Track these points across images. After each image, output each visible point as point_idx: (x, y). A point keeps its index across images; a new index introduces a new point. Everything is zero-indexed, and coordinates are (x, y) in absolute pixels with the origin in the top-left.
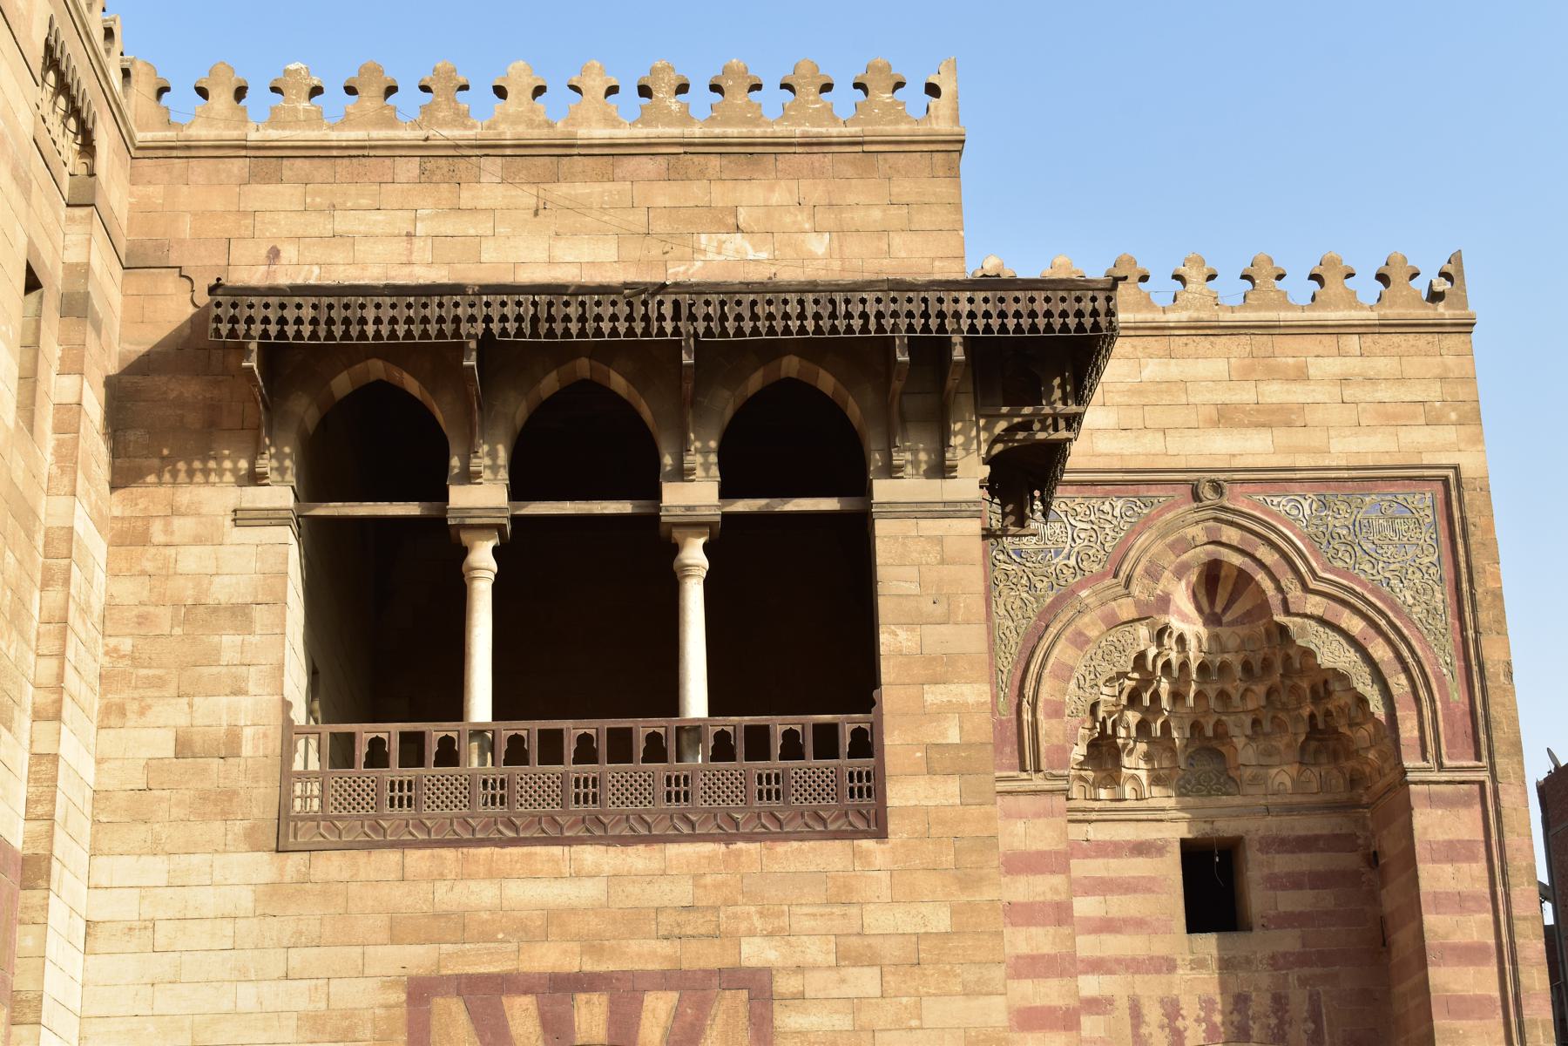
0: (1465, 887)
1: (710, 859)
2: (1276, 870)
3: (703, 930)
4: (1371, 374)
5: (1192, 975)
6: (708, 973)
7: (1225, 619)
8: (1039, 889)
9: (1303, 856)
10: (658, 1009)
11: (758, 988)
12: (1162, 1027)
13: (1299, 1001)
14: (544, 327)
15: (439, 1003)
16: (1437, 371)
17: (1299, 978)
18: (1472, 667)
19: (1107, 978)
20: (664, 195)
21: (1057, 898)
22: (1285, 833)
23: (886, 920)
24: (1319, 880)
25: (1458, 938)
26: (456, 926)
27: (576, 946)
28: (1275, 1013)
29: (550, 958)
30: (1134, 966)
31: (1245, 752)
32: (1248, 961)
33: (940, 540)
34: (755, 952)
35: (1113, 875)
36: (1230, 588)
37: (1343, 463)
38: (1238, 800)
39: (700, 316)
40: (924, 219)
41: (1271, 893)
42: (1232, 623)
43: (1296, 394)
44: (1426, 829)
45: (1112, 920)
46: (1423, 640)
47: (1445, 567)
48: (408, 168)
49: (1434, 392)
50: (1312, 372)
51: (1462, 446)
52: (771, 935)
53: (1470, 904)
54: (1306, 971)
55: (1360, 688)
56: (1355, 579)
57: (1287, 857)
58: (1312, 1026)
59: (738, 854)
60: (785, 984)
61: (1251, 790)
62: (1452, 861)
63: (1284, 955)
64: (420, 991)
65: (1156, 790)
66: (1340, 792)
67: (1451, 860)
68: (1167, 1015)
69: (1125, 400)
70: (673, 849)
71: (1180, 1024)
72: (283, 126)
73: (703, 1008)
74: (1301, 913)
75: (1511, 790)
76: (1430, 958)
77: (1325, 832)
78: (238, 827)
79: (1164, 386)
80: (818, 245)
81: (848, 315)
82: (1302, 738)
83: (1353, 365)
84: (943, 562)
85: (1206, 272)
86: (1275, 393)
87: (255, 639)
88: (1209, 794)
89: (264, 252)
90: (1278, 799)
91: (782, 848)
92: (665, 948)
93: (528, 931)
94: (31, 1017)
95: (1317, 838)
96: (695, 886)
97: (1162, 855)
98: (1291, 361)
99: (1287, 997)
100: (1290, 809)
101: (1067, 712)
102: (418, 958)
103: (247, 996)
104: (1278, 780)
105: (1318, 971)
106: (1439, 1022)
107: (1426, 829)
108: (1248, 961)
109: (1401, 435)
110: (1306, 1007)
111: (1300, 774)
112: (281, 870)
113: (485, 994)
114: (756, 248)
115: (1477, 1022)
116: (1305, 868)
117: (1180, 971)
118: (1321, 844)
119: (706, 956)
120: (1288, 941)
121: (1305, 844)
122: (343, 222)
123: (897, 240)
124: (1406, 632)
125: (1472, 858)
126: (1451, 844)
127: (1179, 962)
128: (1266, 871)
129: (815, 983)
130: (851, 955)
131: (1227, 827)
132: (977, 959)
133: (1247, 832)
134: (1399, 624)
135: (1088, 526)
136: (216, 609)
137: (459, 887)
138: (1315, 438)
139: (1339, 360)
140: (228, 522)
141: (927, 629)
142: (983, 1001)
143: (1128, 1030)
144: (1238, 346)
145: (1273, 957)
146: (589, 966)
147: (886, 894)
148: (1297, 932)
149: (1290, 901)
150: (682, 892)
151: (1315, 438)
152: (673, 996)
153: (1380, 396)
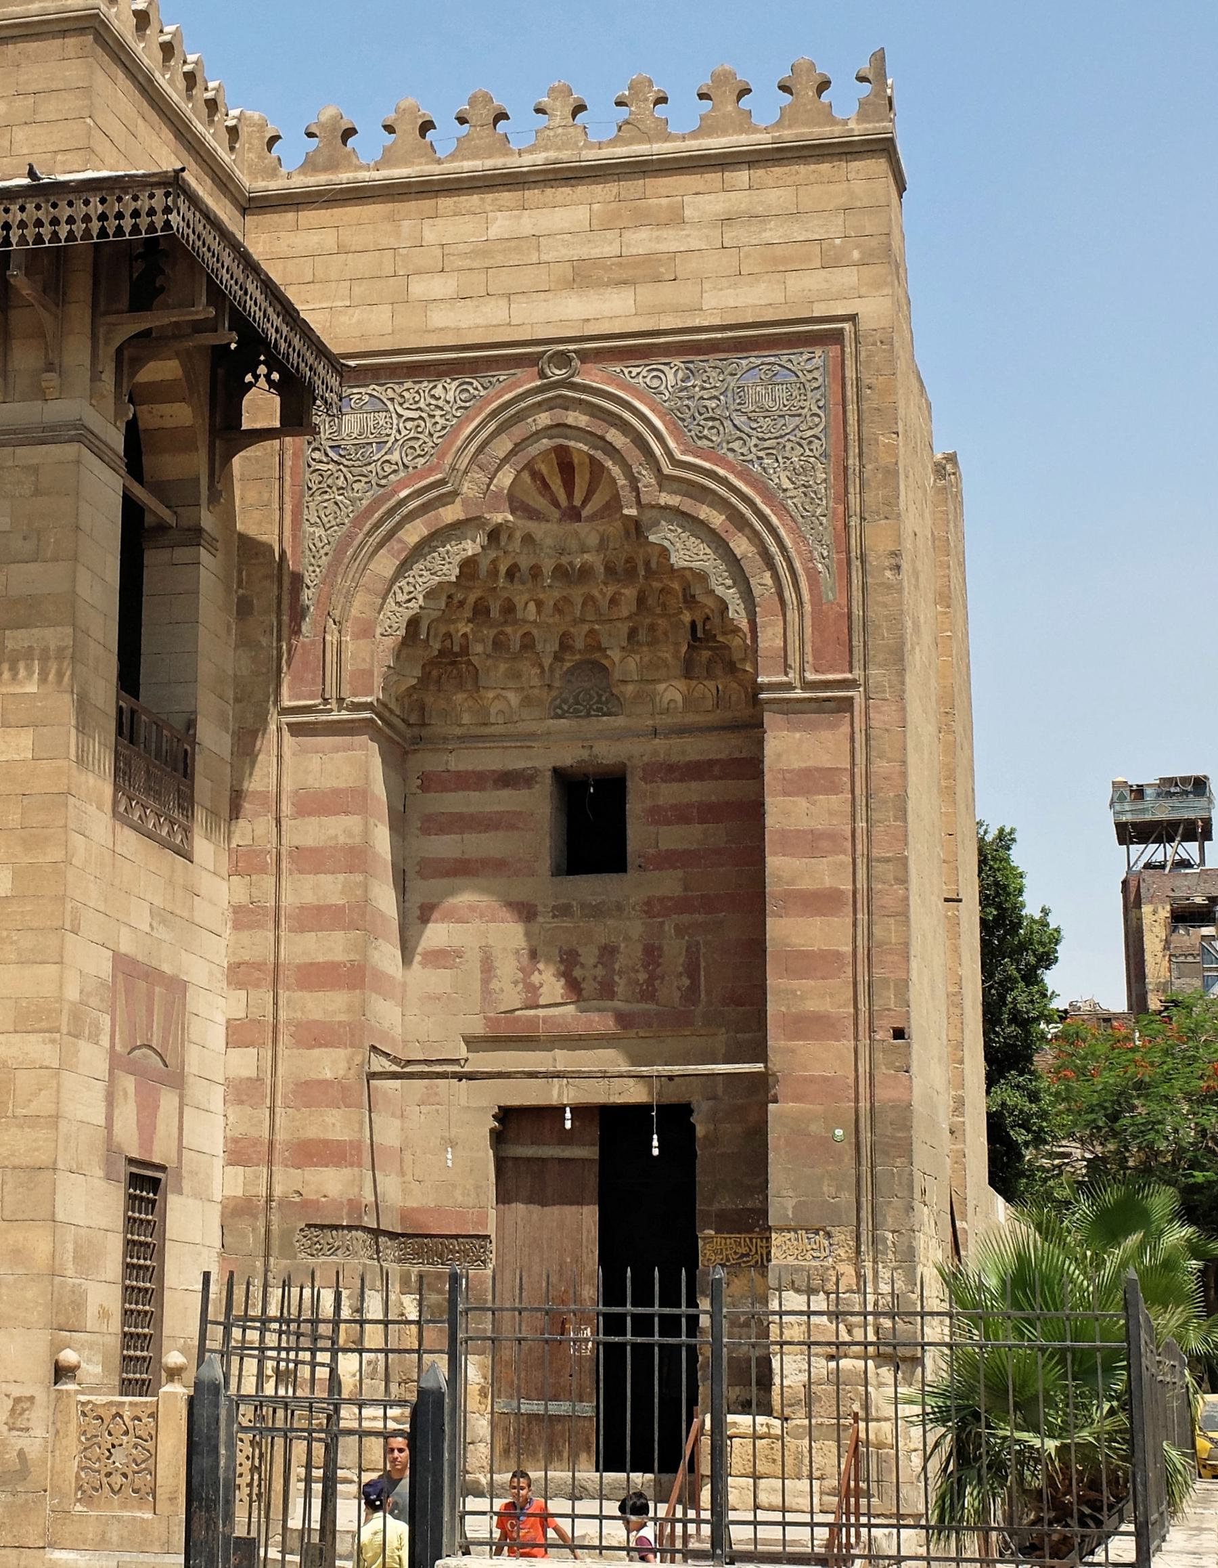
0: (820, 824)
4: (760, 210)
7: (584, 513)
8: (332, 832)
9: (693, 785)
12: (516, 983)
13: (674, 951)
16: (842, 201)
17: (676, 926)
21: (349, 841)
22: (675, 759)
25: (805, 885)
28: (645, 967)
31: (625, 664)
32: (619, 908)
33: (35, 470)
35: (472, 810)
37: (717, 321)
38: (620, 721)
40: (50, 108)
41: (652, 829)
42: (591, 518)
43: (671, 240)
44: (779, 755)
45: (468, 861)
46: (796, 531)
47: (832, 440)
49: (833, 228)
50: (688, 213)
51: (863, 291)
53: (824, 844)
54: (686, 918)
55: (720, 591)
56: (721, 461)
57: (675, 786)
58: (687, 982)
63: (662, 900)
67: (805, 792)
68: (522, 970)
69: (467, 263)
74: (686, 851)
77: (722, 756)
79: (513, 244)
82: (684, 648)
83: (738, 201)
84: (37, 492)
85: (571, 103)
86: (641, 241)
88: (588, 715)
90: (669, 720)
95: (711, 763)
98: (664, 201)
99: (660, 948)
101: (379, 630)
104: (668, 696)
105: (699, 918)
107: (779, 755)
109: (789, 283)
110: (681, 960)
116: (695, 798)
117: (540, 919)
118: (716, 770)
120: (668, 884)
121: (696, 771)
123: (20, 134)
124: (774, 520)
125: (834, 789)
126: (807, 773)
127: (540, 908)
128: (649, 803)
131: (608, 753)
132: (35, 924)
133: (630, 758)
135: (415, 415)
138: (684, 294)
139: (722, 196)
144: (602, 192)
145: (648, 903)
148: (680, 873)
149: (673, 838)
151: (684, 294)
153: (768, 236)
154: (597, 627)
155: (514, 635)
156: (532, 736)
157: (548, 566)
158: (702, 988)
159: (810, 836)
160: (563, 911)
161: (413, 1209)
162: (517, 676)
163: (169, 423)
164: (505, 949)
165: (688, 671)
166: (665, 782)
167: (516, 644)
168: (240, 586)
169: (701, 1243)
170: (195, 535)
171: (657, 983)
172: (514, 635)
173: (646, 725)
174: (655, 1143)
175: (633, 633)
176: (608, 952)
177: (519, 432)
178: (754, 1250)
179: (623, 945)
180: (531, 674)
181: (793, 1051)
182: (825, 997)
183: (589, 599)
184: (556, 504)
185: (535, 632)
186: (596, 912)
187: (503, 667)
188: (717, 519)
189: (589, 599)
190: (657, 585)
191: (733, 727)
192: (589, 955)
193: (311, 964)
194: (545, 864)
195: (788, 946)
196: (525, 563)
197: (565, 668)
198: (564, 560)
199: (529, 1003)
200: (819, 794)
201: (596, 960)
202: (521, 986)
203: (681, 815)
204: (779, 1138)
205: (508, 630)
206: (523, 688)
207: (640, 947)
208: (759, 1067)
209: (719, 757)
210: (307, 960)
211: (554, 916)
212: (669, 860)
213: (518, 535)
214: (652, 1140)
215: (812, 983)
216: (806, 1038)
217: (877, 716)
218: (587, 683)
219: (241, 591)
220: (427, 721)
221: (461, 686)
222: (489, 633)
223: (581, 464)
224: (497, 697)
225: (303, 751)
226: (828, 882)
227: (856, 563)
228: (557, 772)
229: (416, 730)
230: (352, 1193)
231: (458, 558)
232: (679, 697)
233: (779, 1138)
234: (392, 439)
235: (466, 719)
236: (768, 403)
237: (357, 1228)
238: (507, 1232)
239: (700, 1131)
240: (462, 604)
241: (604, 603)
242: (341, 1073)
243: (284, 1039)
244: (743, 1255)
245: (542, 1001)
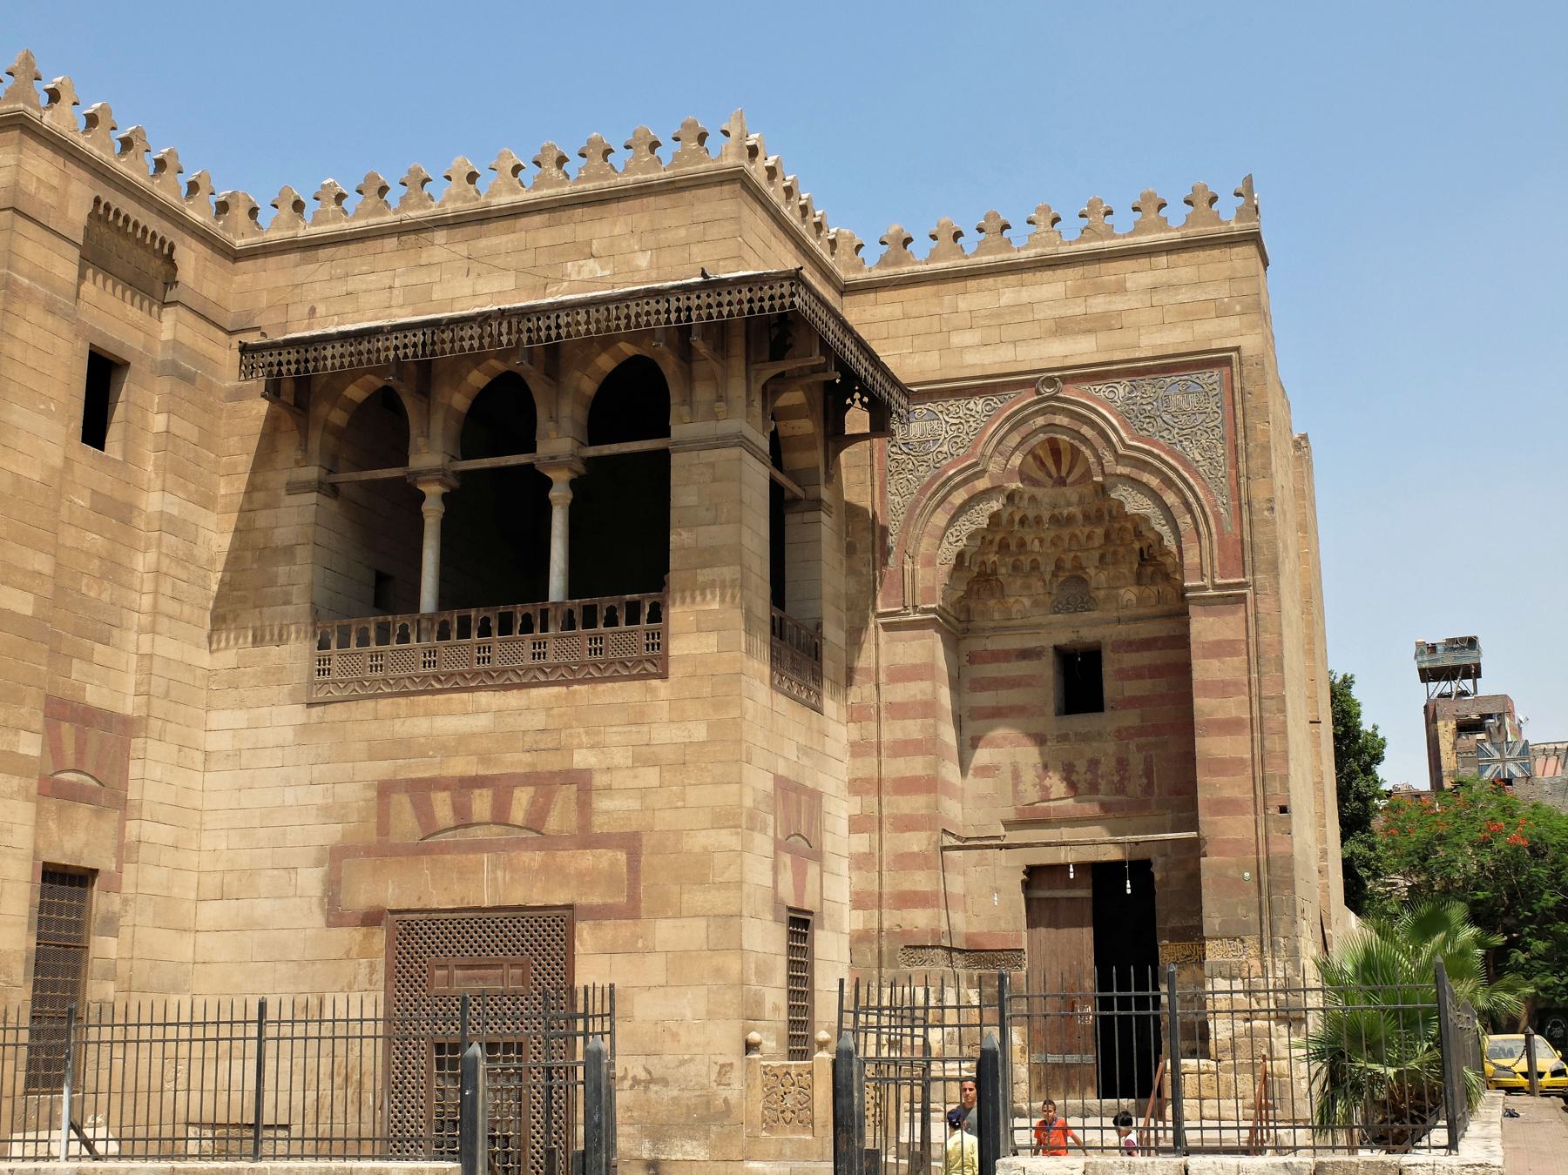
0: (1228, 676)
1: (557, 697)
3: (550, 746)
4: (1175, 281)
5: (1059, 746)
6: (553, 774)
10: (522, 799)
11: (582, 782)
13: (1136, 761)
14: (428, 349)
15: (395, 798)
18: (1241, 505)
20: (545, 237)
23: (665, 734)
25: (1220, 716)
26: (404, 748)
27: (474, 759)
29: (461, 766)
31: (1098, 577)
33: (712, 465)
34: (582, 759)
38: (1095, 615)
39: (525, 329)
40: (714, 232)
42: (1074, 484)
43: (1118, 303)
48: (392, 243)
52: (592, 747)
54: (1143, 740)
55: (1158, 528)
56: (1156, 444)
58: (1144, 781)
59: (575, 693)
60: (600, 780)
63: (1127, 729)
64: (385, 789)
67: (1218, 656)
69: (987, 322)
70: (534, 692)
72: (319, 224)
73: (549, 797)
78: (286, 689)
80: (643, 260)
81: (618, 318)
83: (1160, 276)
84: (714, 480)
85: (1051, 216)
86: (1099, 304)
87: (296, 568)
89: (307, 310)
90: (1127, 612)
91: (601, 687)
92: (527, 758)
93: (447, 748)
94: (136, 815)
95: (1155, 639)
96: (548, 716)
100: (1137, 619)
102: (383, 769)
103: (290, 796)
104: (1126, 597)
105: (1152, 739)
108: (1100, 734)
112: (309, 717)
113: (420, 789)
114: (602, 269)
116: (1147, 662)
119: (553, 763)
120: (1130, 718)
121: (1147, 644)
122: (353, 284)
123: (695, 249)
124: (1191, 481)
126: (1218, 643)
128: (1117, 667)
129: (618, 780)
130: (644, 758)
131: (1089, 635)
134: (1186, 475)
136: (275, 550)
137: (408, 722)
138: (1127, 337)
139: (1150, 273)
140: (283, 493)
141: (701, 529)
142: (726, 787)
143: (1010, 788)
144: (1072, 274)
145: (1118, 731)
146: (482, 771)
147: (665, 716)
148: (1138, 711)
149: (1133, 688)
150: (539, 720)
151: (1127, 337)
152: (531, 789)
153: (1180, 298)
155: (1026, 561)
156: (1039, 626)
157: (1046, 515)
160: (1063, 738)
162: (1028, 587)
163: (798, 432)
165: (1139, 580)
167: (1027, 567)
170: (817, 504)
172: (1026, 561)
173: (1114, 616)
175: (1102, 557)
176: (1094, 763)
177: (1024, 430)
180: (1038, 586)
182: (1235, 787)
183: (1073, 536)
184: (1050, 476)
186: (1085, 738)
187: (1019, 582)
188: (1154, 482)
189: (1073, 536)
191: (1169, 615)
192: (1081, 766)
194: (1051, 708)
196: (1031, 514)
198: (1056, 512)
203: (1138, 673)
205: (1022, 558)
207: (1114, 760)
208: (1193, 834)
212: (1131, 702)
213: (1026, 496)
218: (1074, 591)
221: (992, 595)
222: (1009, 560)
225: (892, 640)
228: (1058, 650)
232: (1133, 598)
235: (997, 616)
236: (1184, 405)
239: (1157, 877)
240: (991, 542)
241: (1083, 539)
243: (886, 826)
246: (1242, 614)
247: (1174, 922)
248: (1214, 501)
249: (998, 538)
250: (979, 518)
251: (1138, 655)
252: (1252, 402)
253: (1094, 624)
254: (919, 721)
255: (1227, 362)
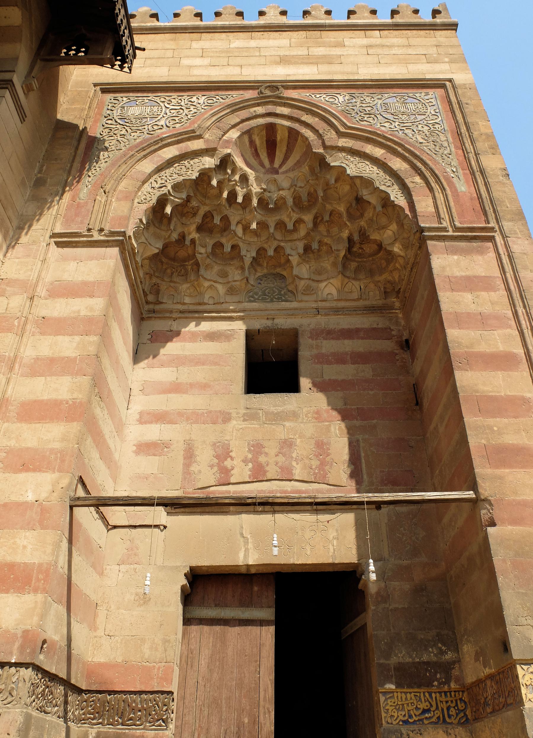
2: (324, 351)
5: (244, 425)
7: (280, 171)
9: (346, 342)
12: (212, 466)
19: (169, 426)
22: (332, 327)
24: (359, 358)
25: (483, 348)
30: (194, 417)
31: (303, 270)
35: (187, 353)
36: (284, 149)
38: (295, 305)
41: (318, 366)
42: (284, 173)
57: (333, 342)
61: (305, 298)
62: (471, 290)
65: (229, 298)
66: (375, 298)
68: (217, 457)
71: (228, 463)
74: (343, 381)
75: (520, 241)
76: (455, 364)
77: (366, 326)
79: (245, 49)
88: (272, 301)
95: (358, 330)
97: (229, 341)
98: (332, 40)
99: (329, 444)
104: (326, 291)
106: (469, 419)
111: (343, 286)
115: (512, 420)
117: (234, 422)
118: (362, 334)
126: (468, 279)
127: (234, 415)
128: (315, 352)
131: (284, 322)
133: (301, 326)
143: (180, 468)
148: (340, 394)
154: (282, 244)
158: (364, 471)
159: (480, 317)
161: (101, 665)
162: (224, 275)
164: (204, 442)
166: (326, 339)
167: (228, 248)
168: (40, 172)
169: (382, 698)
171: (327, 468)
174: (372, 568)
175: (307, 249)
177: (244, 114)
178: (434, 704)
179: (298, 440)
181: (501, 478)
185: (241, 244)
187: (216, 268)
188: (378, 152)
190: (329, 207)
192: (272, 449)
193: (35, 401)
195: (477, 391)
197: (257, 276)
199: (222, 481)
200: (482, 291)
201: (277, 450)
202: (216, 469)
204: (504, 561)
205: (223, 240)
206: (228, 282)
208: (470, 494)
209: (363, 326)
210: (32, 397)
211: (244, 420)
214: (368, 565)
215: (506, 420)
216: (510, 466)
217: (515, 246)
219: (39, 175)
220: (160, 300)
221: (186, 281)
222: (210, 242)
223: (281, 140)
224: (210, 287)
225: (65, 259)
226: (501, 347)
227: (478, 174)
229: (151, 307)
230: (32, 623)
231: (199, 168)
232: (334, 292)
233: (504, 561)
234: (161, 116)
237: (26, 665)
238: (188, 692)
242: (44, 495)
244: (425, 711)
245: (233, 480)
246: (492, 255)
247: (401, 656)
248: (448, 162)
249: (206, 209)
250: (192, 170)
251: (339, 342)
252: (468, 110)
253: (292, 313)
254: (77, 338)
255: (443, 86)
